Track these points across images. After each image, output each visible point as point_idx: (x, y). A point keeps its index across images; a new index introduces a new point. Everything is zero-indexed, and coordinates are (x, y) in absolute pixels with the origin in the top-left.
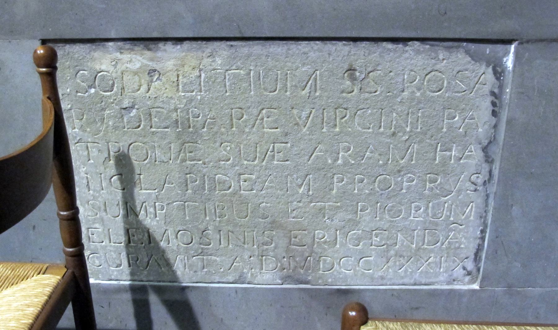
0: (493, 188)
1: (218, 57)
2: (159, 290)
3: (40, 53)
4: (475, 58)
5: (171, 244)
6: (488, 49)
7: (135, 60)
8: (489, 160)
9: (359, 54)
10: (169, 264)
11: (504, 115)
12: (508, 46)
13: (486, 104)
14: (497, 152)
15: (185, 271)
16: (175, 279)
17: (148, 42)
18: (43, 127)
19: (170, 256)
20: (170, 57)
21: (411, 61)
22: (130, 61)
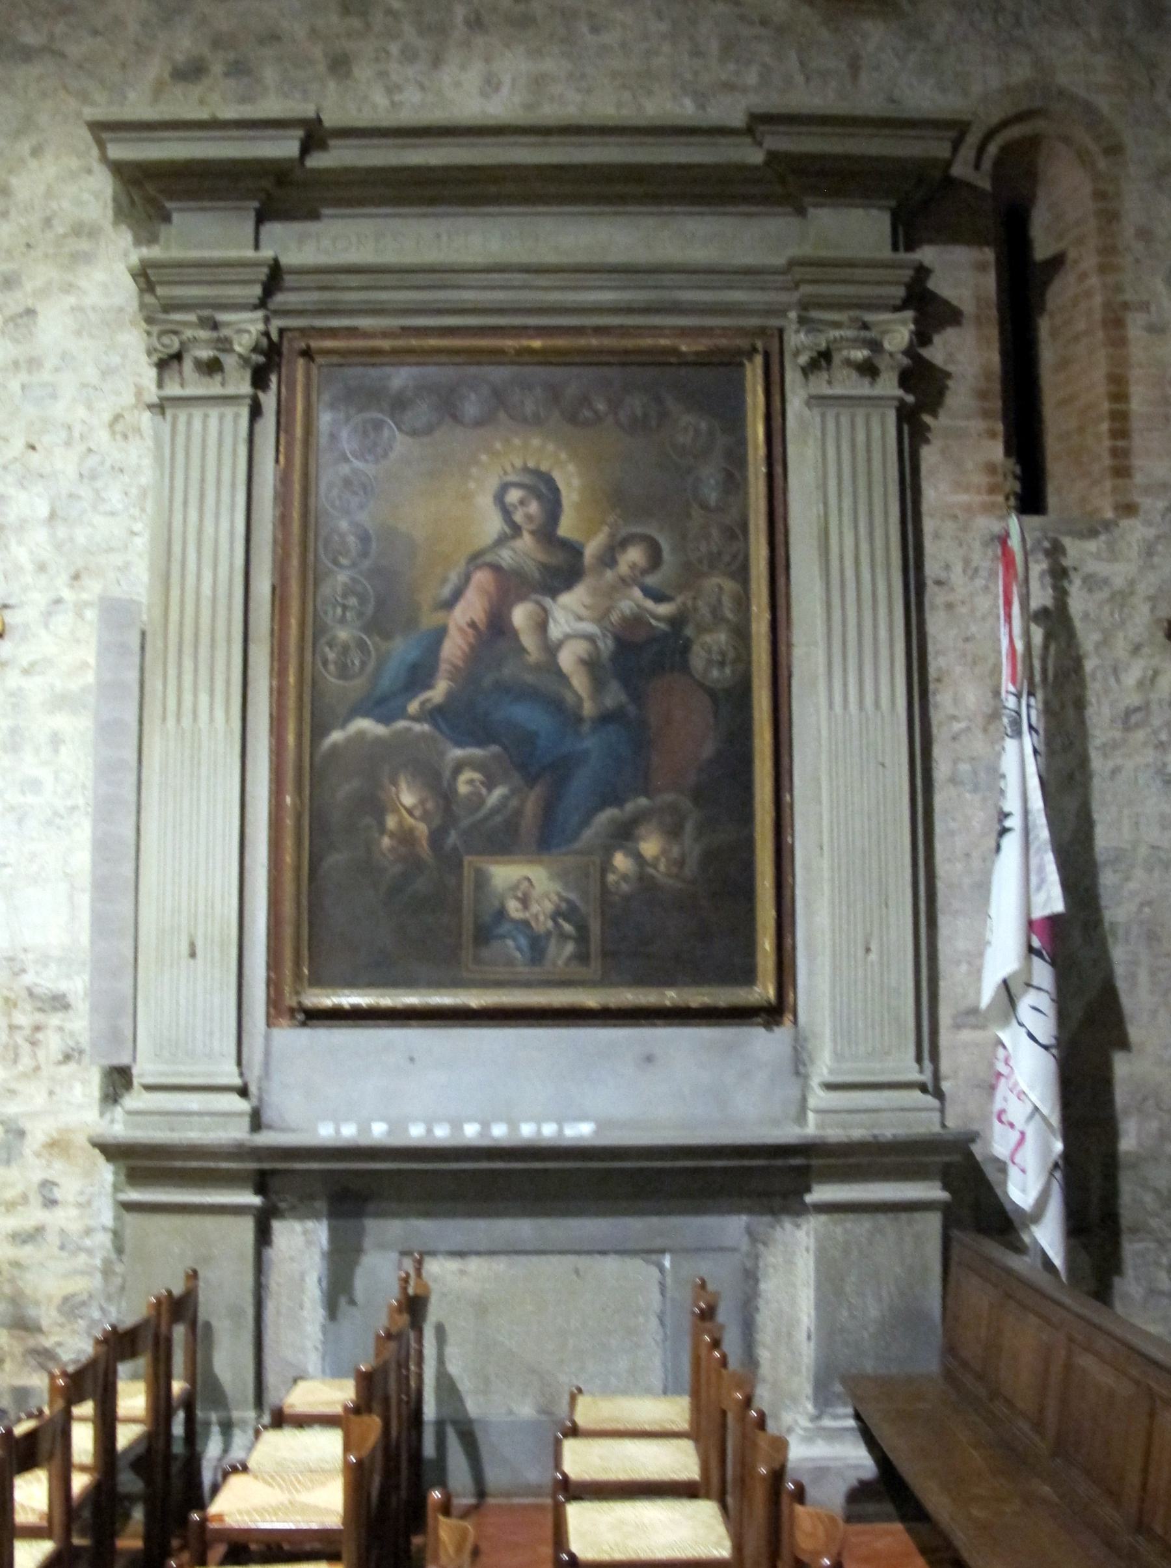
0: (668, 1343)
1: (500, 1265)
2: (455, 1423)
3: (644, 880)
4: (647, 1261)
5: (465, 1385)
6: (654, 1257)
7: (453, 1265)
8: (662, 1323)
9: (582, 1262)
10: (461, 1400)
11: (668, 1295)
12: (660, 1256)
13: (656, 1290)
14: (668, 1321)
15: (473, 1407)
16: (465, 1410)
17: (461, 1254)
18: (377, 1355)
19: (464, 1395)
20: (474, 1265)
21: (610, 1265)
22: (69, 428)
